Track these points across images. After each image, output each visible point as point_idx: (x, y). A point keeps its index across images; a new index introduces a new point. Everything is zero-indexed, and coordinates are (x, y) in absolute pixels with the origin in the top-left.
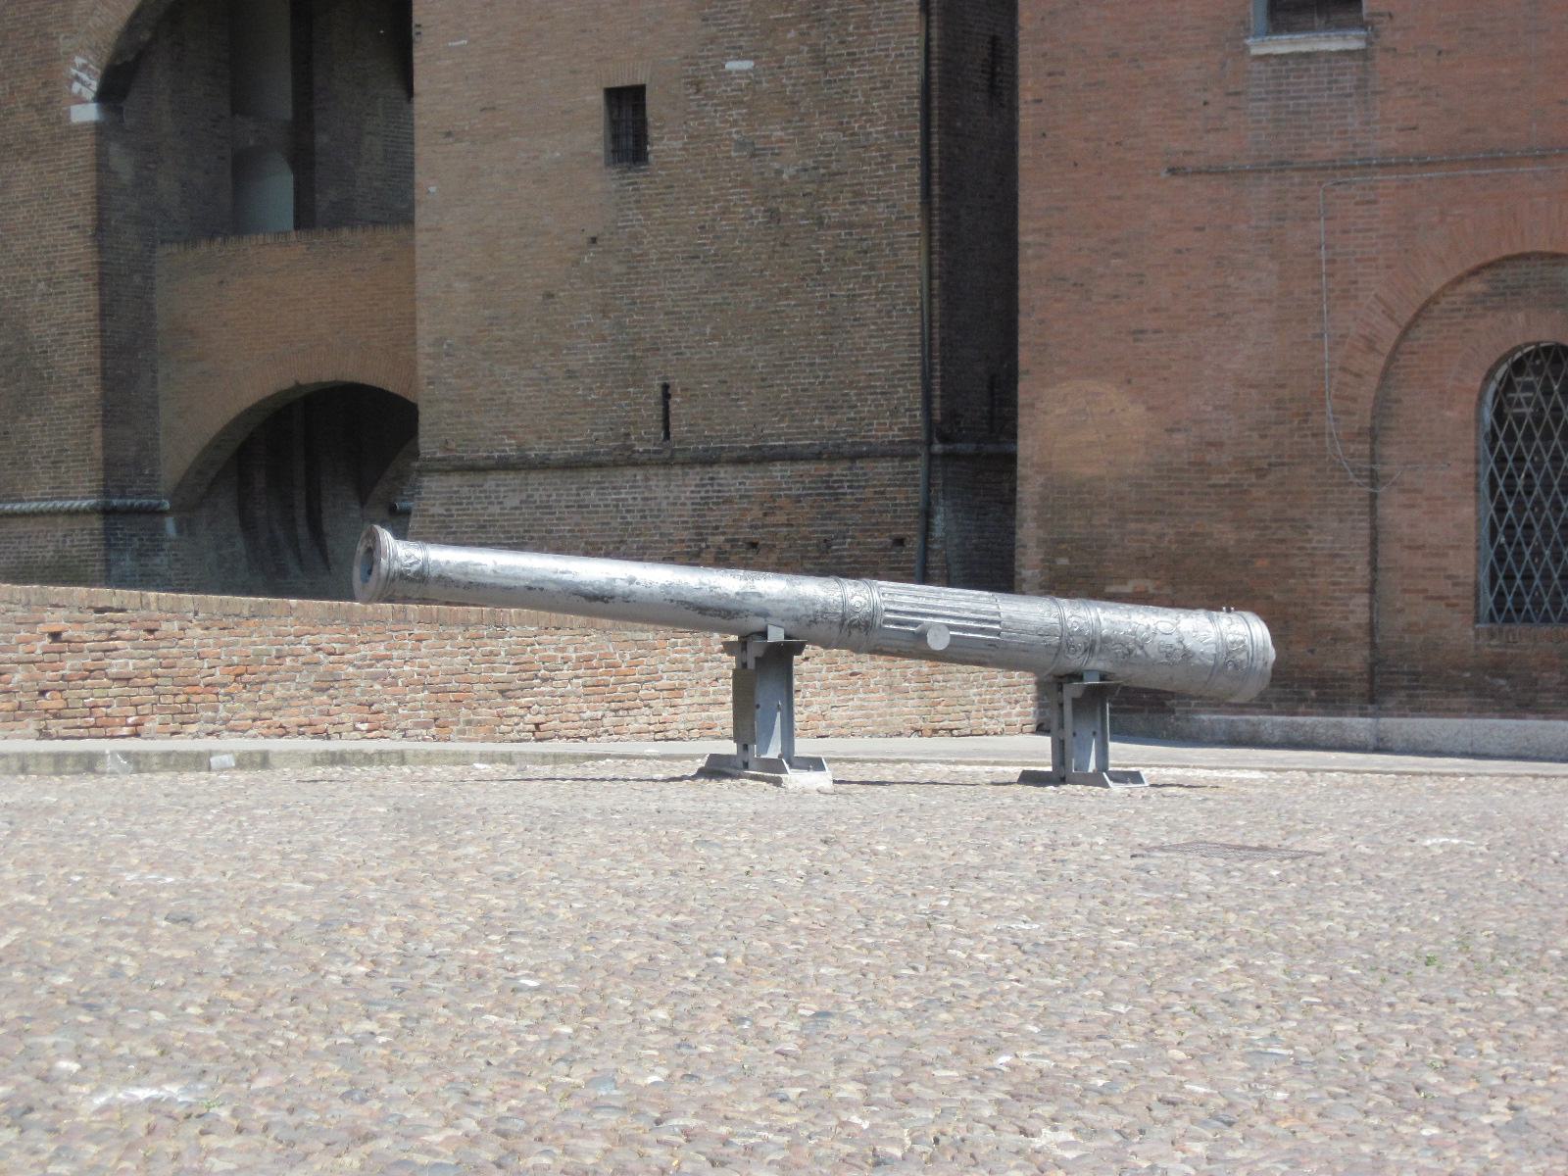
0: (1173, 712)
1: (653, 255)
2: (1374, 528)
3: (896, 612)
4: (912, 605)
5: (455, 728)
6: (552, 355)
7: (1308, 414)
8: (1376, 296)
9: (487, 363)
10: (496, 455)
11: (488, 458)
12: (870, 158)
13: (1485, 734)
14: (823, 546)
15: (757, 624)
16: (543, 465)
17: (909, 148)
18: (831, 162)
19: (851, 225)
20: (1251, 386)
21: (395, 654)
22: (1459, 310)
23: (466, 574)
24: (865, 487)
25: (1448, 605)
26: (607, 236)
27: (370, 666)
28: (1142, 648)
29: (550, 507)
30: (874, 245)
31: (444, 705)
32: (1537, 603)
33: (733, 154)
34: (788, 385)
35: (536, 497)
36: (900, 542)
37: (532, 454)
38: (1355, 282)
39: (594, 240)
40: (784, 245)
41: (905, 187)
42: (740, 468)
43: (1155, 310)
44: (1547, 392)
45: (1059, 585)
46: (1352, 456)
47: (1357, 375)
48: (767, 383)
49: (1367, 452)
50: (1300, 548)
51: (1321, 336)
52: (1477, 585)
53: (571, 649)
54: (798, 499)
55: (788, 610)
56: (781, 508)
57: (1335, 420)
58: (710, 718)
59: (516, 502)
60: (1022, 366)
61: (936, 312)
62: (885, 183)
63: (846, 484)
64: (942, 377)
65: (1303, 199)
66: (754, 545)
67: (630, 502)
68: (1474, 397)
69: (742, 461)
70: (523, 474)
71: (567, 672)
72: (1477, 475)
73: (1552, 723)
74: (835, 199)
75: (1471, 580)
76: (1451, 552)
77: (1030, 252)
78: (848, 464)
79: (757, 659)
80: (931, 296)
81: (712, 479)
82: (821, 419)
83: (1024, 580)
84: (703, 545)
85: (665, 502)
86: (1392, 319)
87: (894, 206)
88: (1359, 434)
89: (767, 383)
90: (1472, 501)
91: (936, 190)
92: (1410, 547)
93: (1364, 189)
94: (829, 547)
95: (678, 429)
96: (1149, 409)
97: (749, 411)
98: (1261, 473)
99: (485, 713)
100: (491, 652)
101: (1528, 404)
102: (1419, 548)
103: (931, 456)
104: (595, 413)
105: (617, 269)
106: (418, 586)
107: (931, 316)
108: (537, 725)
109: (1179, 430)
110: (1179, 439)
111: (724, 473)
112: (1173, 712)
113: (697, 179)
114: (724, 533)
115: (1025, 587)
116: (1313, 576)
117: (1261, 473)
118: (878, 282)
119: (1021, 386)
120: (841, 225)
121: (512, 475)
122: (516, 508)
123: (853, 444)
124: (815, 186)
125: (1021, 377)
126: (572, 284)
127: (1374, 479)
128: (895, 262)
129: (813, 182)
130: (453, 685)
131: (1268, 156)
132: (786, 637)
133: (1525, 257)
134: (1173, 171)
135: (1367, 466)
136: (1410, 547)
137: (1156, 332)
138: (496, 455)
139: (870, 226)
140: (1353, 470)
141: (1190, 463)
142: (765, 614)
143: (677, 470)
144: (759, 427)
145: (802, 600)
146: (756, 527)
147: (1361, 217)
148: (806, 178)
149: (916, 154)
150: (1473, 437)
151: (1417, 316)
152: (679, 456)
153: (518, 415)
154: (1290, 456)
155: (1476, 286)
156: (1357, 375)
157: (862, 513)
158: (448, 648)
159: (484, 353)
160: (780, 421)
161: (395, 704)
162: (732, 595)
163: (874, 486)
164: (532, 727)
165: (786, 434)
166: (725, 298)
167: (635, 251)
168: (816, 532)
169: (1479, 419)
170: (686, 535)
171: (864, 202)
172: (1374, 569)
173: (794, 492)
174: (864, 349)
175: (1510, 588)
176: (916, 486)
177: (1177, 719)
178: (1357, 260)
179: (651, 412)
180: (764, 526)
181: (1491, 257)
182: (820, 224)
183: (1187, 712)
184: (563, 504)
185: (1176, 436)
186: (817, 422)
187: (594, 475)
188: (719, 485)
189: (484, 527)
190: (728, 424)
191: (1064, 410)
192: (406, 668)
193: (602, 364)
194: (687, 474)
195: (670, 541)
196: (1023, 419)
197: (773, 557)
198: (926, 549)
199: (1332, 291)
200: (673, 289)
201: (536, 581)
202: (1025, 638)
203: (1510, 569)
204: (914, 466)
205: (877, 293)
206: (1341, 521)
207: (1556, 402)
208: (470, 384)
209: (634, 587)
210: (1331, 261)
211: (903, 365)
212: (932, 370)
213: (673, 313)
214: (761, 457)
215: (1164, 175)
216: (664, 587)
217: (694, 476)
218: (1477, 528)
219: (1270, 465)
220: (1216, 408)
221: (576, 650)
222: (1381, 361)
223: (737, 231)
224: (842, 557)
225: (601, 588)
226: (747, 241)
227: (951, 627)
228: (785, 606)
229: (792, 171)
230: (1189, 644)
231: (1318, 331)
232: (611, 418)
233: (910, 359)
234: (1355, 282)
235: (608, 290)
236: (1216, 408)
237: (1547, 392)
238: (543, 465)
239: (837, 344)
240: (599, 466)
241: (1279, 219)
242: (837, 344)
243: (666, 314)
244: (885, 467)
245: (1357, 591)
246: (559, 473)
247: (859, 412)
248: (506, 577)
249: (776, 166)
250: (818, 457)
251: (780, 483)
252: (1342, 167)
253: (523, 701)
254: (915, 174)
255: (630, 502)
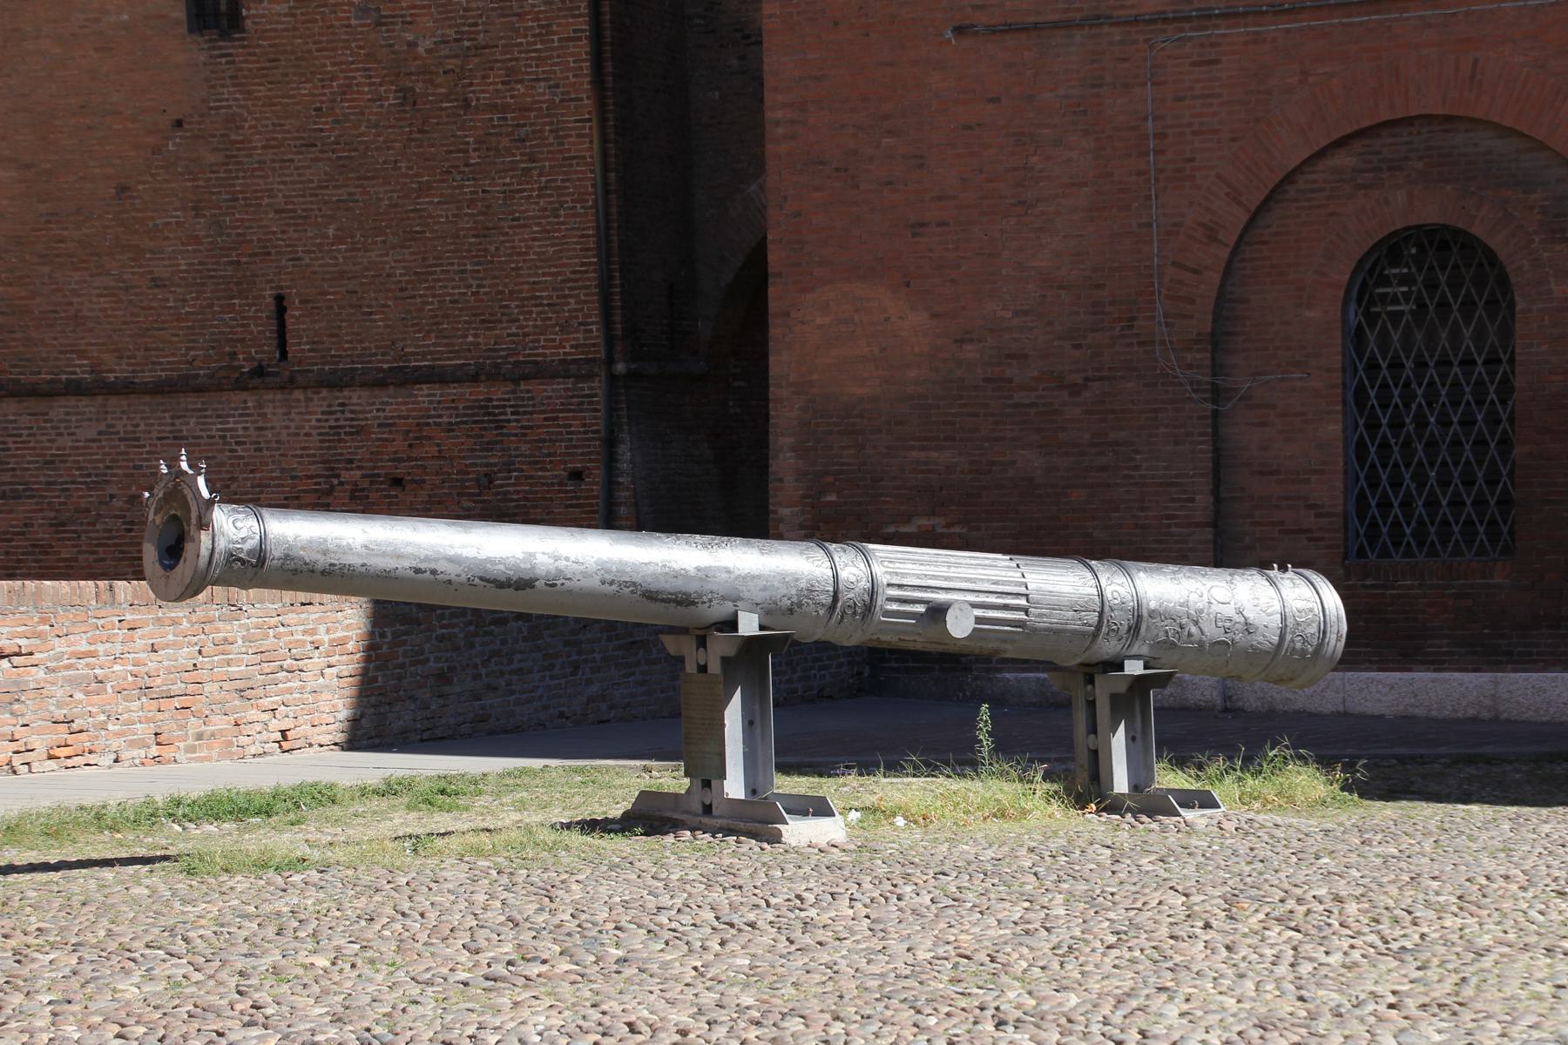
0: (971, 670)
1: (257, 140)
2: (1216, 451)
3: (900, 586)
4: (918, 576)
5: (182, 745)
6: (133, 260)
7: (1133, 319)
8: (1218, 176)
9: (46, 269)
10: (64, 377)
11: (52, 381)
12: (526, 28)
13: (1361, 690)
14: (484, 481)
15: (720, 611)
16: (126, 388)
17: (574, 16)
18: (477, 32)
19: (505, 108)
20: (1060, 288)
21: (101, 648)
22: (1321, 190)
23: (325, 552)
24: (531, 413)
25: (1310, 540)
26: (197, 118)
27: (68, 667)
28: (1196, 623)
29: (138, 439)
30: (534, 132)
31: (167, 715)
32: (1420, 536)
33: (353, 22)
34: (434, 296)
35: (119, 426)
36: (577, 475)
37: (112, 376)
38: (1192, 160)
39: (179, 124)
40: (421, 131)
41: (571, 64)
42: (377, 392)
43: (940, 198)
44: (1432, 286)
45: (824, 528)
46: (1190, 367)
47: (1195, 271)
48: (406, 294)
49: (1208, 362)
50: (1126, 477)
51: (1150, 225)
52: (1345, 515)
53: (322, 629)
54: (450, 428)
55: (765, 589)
56: (429, 438)
57: (1167, 325)
58: (483, 707)
59: (92, 434)
60: (772, 268)
61: (614, 210)
62: (544, 59)
63: (509, 410)
64: (622, 286)
65: (1125, 60)
66: (397, 482)
67: (240, 432)
68: (1341, 294)
69: (381, 384)
70: (100, 399)
71: (318, 661)
72: (1344, 385)
73: (1446, 675)
74: (484, 77)
75: (1340, 509)
76: (1314, 478)
77: (780, 131)
78: (511, 387)
79: (725, 661)
80: (606, 192)
81: (343, 405)
82: (475, 336)
83: (781, 520)
84: (336, 481)
85: (285, 432)
86: (1239, 203)
87: (557, 86)
88: (1197, 342)
89: (406, 294)
90: (1340, 416)
91: (609, 67)
92: (1260, 473)
93: (1202, 45)
94: (491, 482)
95: (299, 347)
96: (934, 316)
97: (386, 326)
98: (1075, 390)
99: (220, 723)
100: (226, 639)
101: (1407, 301)
102: (1272, 473)
103: (612, 378)
104: (192, 328)
105: (211, 158)
106: (254, 569)
107: (607, 214)
108: (283, 732)
109: (971, 341)
110: (970, 352)
111: (357, 398)
112: (971, 670)
113: (309, 51)
114: (359, 468)
115: (782, 527)
116: (1142, 509)
117: (1075, 390)
118: (540, 175)
119: (772, 291)
120: (493, 108)
121: (85, 401)
122: (93, 441)
123: (516, 364)
124: (457, 62)
125: (771, 280)
126: (153, 175)
127: (1217, 394)
128: (561, 152)
129: (456, 56)
130: (178, 688)
131: (1080, 10)
132: (762, 628)
133: (1407, 121)
134: (959, 30)
135: (1208, 379)
136: (1260, 473)
137: (939, 225)
138: (64, 377)
139: (529, 110)
140: (1191, 383)
141: (986, 380)
142: (736, 599)
143: (298, 394)
144: (400, 345)
145: (783, 577)
146: (401, 460)
147: (1198, 80)
148: (447, 52)
149: (583, 24)
150: (1339, 341)
151: (1268, 198)
152: (300, 379)
153: (91, 330)
154: (1110, 369)
155: (1344, 160)
156: (1195, 271)
157: (529, 442)
158: (171, 637)
159: (41, 256)
160: (424, 339)
161: (103, 718)
162: (692, 572)
163: (543, 412)
164: (278, 736)
165: (431, 353)
166: (350, 194)
167: (233, 137)
168: (475, 465)
169: (1345, 321)
170: (314, 469)
171: (520, 81)
172: (1218, 501)
173: (445, 419)
174: (527, 254)
175: (1385, 517)
176: (597, 410)
177: (976, 678)
178: (1194, 133)
179: (261, 327)
180: (410, 459)
181: (1366, 123)
182: (466, 104)
183: (988, 670)
184: (154, 435)
185: (968, 347)
186: (470, 339)
187: (191, 401)
188: (352, 412)
189: (52, 462)
190: (361, 342)
191: (827, 320)
192: (117, 668)
193: (197, 271)
194: (311, 400)
195: (293, 478)
196: (775, 331)
197: (423, 495)
198: (611, 484)
199: (1162, 171)
200: (284, 183)
201: (427, 559)
202: (1055, 619)
203: (1432, 493)
204: (591, 388)
205: (540, 189)
206: (1176, 443)
207: (1443, 295)
208: (23, 294)
209: (562, 564)
210: (1160, 136)
211: (574, 272)
212: (611, 278)
213: (283, 211)
214: (404, 378)
215: (949, 34)
216: (600, 563)
217: (320, 401)
218: (1346, 447)
219: (1086, 379)
220: (1016, 313)
221: (328, 631)
222: (1225, 254)
223: (363, 114)
224: (506, 493)
225: (517, 568)
226: (376, 126)
227: (975, 606)
228: (762, 583)
229: (428, 43)
230: (1251, 615)
231: (1144, 220)
232: (213, 334)
233: (583, 264)
234: (1192, 160)
235: (201, 183)
236: (1016, 313)
237: (1432, 286)
238: (126, 388)
239: (492, 248)
240: (199, 390)
241: (1093, 86)
242: (492, 248)
243: (277, 212)
244: (553, 391)
245: (1198, 525)
246: (148, 398)
247: (522, 327)
248: (384, 555)
249: (409, 37)
250: (475, 378)
251: (428, 409)
252: (1175, 19)
253: (266, 703)
254: (583, 48)
255: (240, 432)
